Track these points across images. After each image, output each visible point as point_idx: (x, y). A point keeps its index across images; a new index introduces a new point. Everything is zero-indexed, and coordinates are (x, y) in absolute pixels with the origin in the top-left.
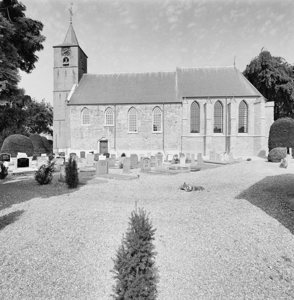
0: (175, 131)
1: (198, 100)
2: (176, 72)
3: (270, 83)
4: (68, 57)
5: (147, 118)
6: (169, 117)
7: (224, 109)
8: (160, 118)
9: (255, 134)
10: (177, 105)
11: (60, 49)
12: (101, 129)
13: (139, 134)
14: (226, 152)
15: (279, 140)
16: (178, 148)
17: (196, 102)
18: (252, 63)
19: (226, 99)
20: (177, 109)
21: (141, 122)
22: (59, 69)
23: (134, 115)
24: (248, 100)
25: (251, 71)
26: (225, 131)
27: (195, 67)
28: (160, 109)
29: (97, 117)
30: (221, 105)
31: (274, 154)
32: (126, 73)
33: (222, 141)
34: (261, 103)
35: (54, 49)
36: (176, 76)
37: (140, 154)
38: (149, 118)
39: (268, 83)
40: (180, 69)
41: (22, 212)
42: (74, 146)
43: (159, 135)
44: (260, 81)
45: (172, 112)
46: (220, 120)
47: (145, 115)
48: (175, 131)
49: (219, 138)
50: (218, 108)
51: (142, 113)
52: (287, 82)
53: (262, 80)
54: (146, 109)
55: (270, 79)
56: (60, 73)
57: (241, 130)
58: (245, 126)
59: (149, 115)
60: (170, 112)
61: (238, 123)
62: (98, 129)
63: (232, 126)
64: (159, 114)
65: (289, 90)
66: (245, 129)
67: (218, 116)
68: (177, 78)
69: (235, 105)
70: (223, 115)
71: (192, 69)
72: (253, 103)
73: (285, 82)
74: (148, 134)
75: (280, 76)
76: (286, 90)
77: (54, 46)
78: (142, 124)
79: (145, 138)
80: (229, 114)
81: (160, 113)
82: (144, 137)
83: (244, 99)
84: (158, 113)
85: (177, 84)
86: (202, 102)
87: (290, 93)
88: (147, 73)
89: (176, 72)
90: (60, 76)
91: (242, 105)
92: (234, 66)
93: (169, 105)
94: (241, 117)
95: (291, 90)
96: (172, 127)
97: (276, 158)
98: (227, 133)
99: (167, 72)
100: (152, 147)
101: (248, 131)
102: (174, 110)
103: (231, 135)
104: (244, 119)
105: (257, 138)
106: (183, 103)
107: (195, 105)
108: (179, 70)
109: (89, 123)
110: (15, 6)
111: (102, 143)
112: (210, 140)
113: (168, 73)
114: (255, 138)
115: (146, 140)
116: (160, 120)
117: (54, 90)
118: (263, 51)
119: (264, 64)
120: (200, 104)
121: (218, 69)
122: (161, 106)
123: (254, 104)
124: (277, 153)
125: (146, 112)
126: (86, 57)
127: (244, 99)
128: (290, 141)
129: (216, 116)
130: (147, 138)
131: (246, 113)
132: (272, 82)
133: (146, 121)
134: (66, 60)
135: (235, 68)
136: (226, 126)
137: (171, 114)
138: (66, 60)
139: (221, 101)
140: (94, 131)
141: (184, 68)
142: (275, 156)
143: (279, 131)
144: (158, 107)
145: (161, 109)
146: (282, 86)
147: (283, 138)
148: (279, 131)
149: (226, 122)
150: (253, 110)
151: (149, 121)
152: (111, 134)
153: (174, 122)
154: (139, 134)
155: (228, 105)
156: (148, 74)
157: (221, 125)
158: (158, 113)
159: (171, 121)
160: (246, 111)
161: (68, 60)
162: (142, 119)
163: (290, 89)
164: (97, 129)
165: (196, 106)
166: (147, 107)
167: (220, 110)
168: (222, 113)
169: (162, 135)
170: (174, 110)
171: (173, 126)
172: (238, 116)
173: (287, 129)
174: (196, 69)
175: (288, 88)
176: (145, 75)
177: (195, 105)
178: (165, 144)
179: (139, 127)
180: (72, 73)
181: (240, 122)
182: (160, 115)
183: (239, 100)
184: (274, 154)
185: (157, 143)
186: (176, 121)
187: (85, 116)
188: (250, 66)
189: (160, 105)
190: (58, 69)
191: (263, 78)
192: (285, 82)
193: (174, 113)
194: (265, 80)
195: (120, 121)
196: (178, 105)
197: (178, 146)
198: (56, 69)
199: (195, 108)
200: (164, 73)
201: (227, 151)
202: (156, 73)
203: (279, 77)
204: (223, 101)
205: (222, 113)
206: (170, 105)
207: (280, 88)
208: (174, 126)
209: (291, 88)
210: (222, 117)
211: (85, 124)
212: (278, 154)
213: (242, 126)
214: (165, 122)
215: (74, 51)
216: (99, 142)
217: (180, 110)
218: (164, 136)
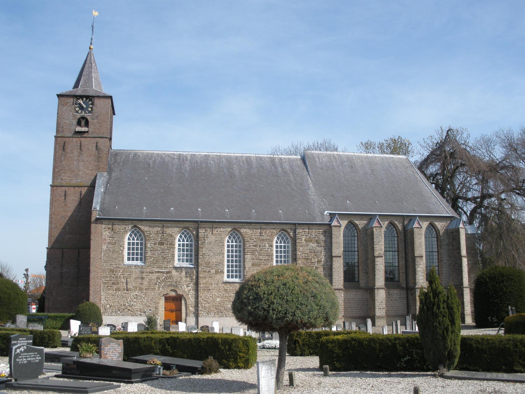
11: (71, 100)
12: (167, 273)
22: (67, 139)
62: (162, 272)
102: (314, 238)
110: (186, 175)
111: (55, 188)
117: (53, 181)
133: (261, 257)
134: (83, 123)
138: (83, 123)
156: (248, 159)
157: (354, 236)
161: (87, 124)
180: (94, 148)
187: (133, 244)
190: (64, 139)
193: (315, 245)
198: (59, 139)
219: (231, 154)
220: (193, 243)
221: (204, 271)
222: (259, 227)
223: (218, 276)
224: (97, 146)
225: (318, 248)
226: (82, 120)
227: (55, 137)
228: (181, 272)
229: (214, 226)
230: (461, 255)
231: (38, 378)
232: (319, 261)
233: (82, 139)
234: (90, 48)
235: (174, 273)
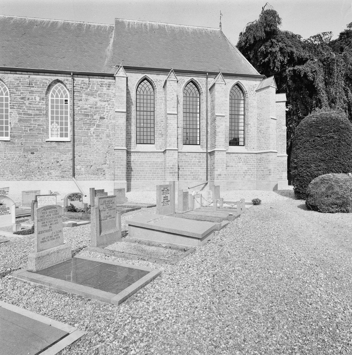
0: (101, 139)
1: (151, 76)
2: (113, 27)
3: (278, 64)
5: (34, 106)
6: (86, 107)
7: (203, 96)
8: (66, 108)
9: (259, 147)
10: (103, 80)
13: (14, 144)
14: (207, 184)
15: (318, 156)
16: (107, 176)
17: (148, 81)
18: (249, 29)
19: (207, 79)
20: (105, 88)
21: (19, 114)
24: (245, 83)
25: (246, 42)
26: (205, 140)
27: (151, 23)
28: (65, 88)
30: (196, 89)
31: (324, 190)
32: (7, 17)
33: (200, 162)
34: (270, 88)
36: (113, 31)
37: (23, 192)
38: (38, 106)
39: (274, 63)
40: (123, 22)
43: (62, 147)
44: (261, 61)
45: (92, 95)
46: (194, 119)
47: (28, 99)
48: (101, 139)
49: (194, 155)
50: (191, 95)
51: (22, 93)
52: (307, 60)
53: (264, 59)
54: (30, 84)
55: (280, 57)
57: (234, 142)
58: (241, 136)
59: (38, 99)
60: (89, 95)
61: (228, 125)
63: (218, 130)
64: (64, 99)
65: (310, 74)
66: (241, 140)
67: (191, 112)
68: (113, 36)
69: (224, 88)
70: (202, 110)
71: (145, 25)
72: (255, 89)
73: (302, 61)
74: (35, 143)
75: (294, 50)
76: (305, 74)
78: (20, 120)
79: (30, 153)
80: (213, 108)
81: (66, 96)
82: (25, 151)
83: (240, 81)
84: (62, 96)
85: (111, 45)
86: (157, 79)
87: (312, 79)
88: (53, 23)
89: (113, 27)
91: (235, 93)
92: (219, 30)
93: (86, 80)
94: (233, 116)
95: (314, 73)
96: (92, 129)
97: (331, 200)
98: (209, 146)
99: (96, 24)
100: (46, 173)
101: (246, 141)
103: (215, 149)
104: (238, 119)
105: (264, 155)
106: (116, 75)
107: (145, 86)
108: (119, 23)
109: (7, 135)
112: (174, 159)
113: (98, 26)
114: (259, 155)
115: (30, 156)
116: (66, 113)
118: (265, 10)
119: (268, 29)
120: (155, 84)
121: (192, 31)
122: (67, 80)
123: (256, 91)
124: (333, 189)
125: (32, 92)
127: (240, 81)
128: (342, 160)
129: (188, 111)
130: (33, 153)
131: (242, 109)
132: (282, 62)
133: (30, 112)
135: (221, 32)
136: (207, 132)
137: (92, 100)
139: (197, 81)
141: (131, 21)
142: (327, 196)
143: (318, 137)
144: (62, 82)
145: (68, 88)
146: (297, 67)
147: (328, 152)
148: (318, 137)
149: (207, 123)
150: (255, 103)
151: (38, 112)
153: (97, 117)
154: (14, 144)
155: (210, 89)
158: (62, 96)
159: (91, 115)
160: (242, 105)
162: (20, 107)
163: (312, 72)
165: (147, 89)
166: (33, 79)
167: (195, 99)
168: (200, 105)
169: (70, 145)
170: (97, 91)
171: (95, 127)
172: (228, 112)
173: (334, 131)
174: (152, 25)
175: (309, 70)
176: (44, 23)
177: (145, 86)
178: (77, 167)
179: (12, 125)
181: (231, 126)
182: (66, 101)
183: (232, 82)
184: (324, 190)
185: (58, 164)
186: (102, 115)
188: (245, 34)
189: (65, 78)
191: (265, 55)
192: (302, 61)
193: (97, 99)
194: (269, 59)
196: (107, 81)
197: (106, 170)
199: (145, 93)
200: (90, 25)
201: (209, 180)
202: (73, 24)
203: (292, 53)
204: (201, 80)
205: (200, 105)
206: (87, 79)
207: (294, 71)
208: (98, 126)
209: (314, 70)
210: (200, 113)
212: (335, 190)
213: (236, 137)
214: (77, 118)
217: (110, 91)
218: (75, 148)
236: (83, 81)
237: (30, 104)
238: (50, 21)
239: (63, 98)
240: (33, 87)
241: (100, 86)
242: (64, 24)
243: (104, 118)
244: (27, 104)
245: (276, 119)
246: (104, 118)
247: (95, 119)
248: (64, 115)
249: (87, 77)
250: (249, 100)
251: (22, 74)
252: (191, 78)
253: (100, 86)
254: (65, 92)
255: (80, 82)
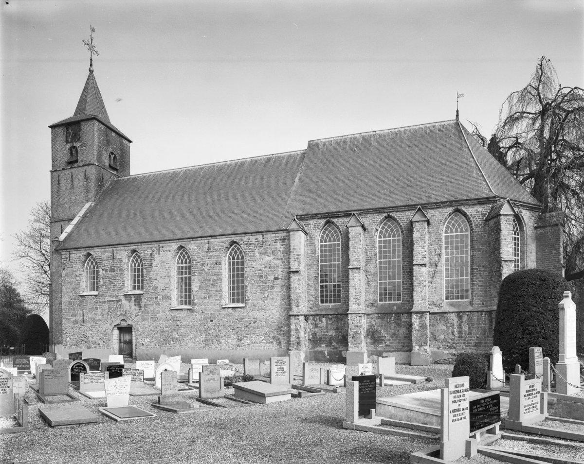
4: (77, 145)
5: (213, 271)
23: (186, 267)
29: (110, 273)
35: (52, 131)
38: (216, 271)
41: (426, 455)
42: (68, 339)
56: (62, 181)
77: (51, 124)
90: (62, 188)
111: (53, 224)
126: (125, 141)
130: (211, 321)
140: (106, 306)
152: (137, 311)
164: (110, 301)
186: (276, 276)
193: (272, 257)
195: (155, 281)
198: (55, 174)
211: (326, 302)
215: (92, 134)
216: (116, 332)
219: (384, 132)
220: (401, 238)
221: (151, 298)
222: (207, 241)
223: (165, 304)
224: (85, 175)
225: (275, 261)
226: (73, 149)
227: (51, 172)
228: (131, 300)
229: (161, 245)
230: (500, 257)
231: (495, 345)
232: (276, 279)
233: (72, 170)
234: (90, 71)
235: (124, 302)
236: (257, 239)
237: (209, 270)
238: (238, 162)
239: (235, 259)
240: (212, 252)
241: (274, 242)
242: (251, 162)
243: (279, 279)
244: (206, 270)
245: (179, 390)
246: (279, 279)
247: (269, 281)
248: (332, 258)
249: (261, 234)
250: (475, 233)
251: (169, 243)
252: (180, 243)
253: (274, 242)
254: (337, 236)
255: (254, 240)
